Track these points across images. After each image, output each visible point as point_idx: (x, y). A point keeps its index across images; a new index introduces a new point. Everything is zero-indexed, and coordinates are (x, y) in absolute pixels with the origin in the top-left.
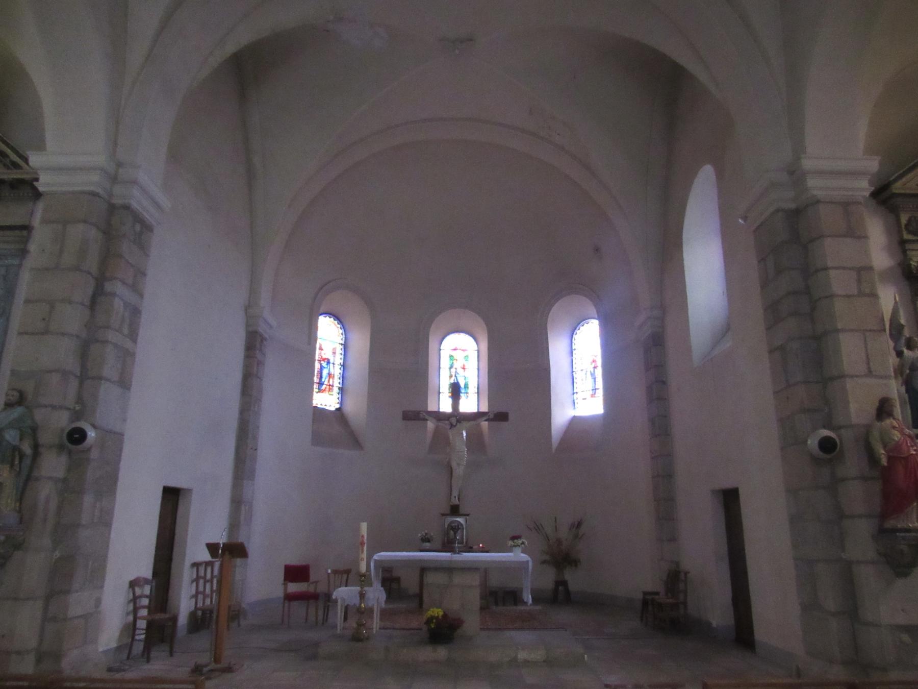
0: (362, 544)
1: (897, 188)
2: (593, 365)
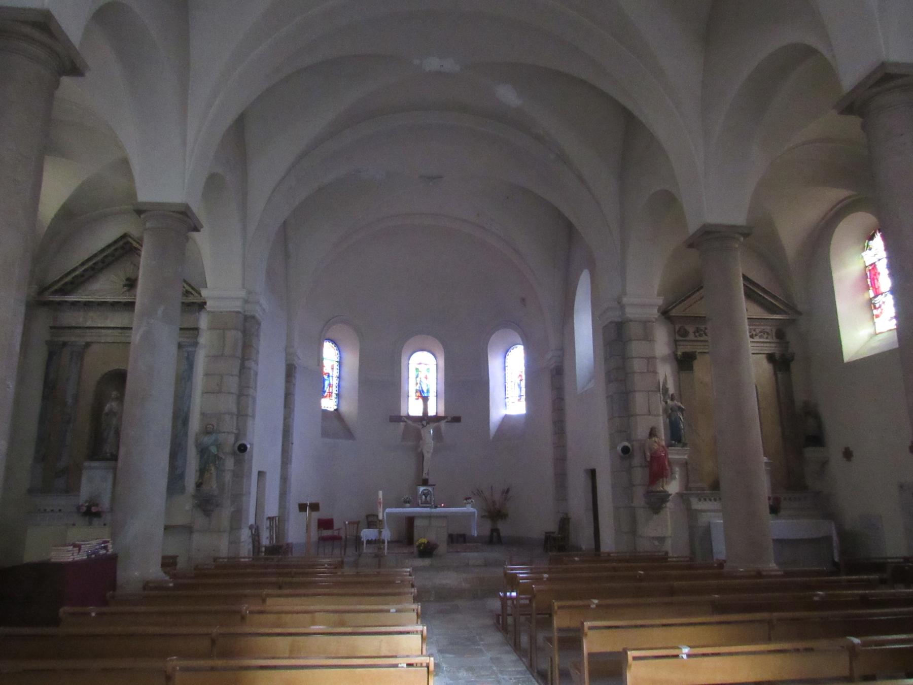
0: (380, 503)
1: (673, 313)
2: (520, 378)
